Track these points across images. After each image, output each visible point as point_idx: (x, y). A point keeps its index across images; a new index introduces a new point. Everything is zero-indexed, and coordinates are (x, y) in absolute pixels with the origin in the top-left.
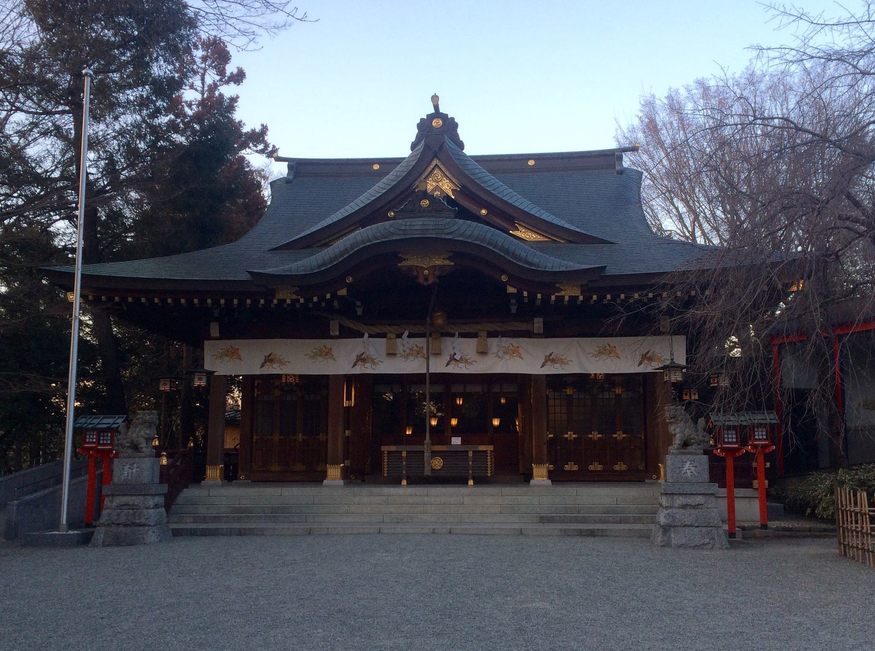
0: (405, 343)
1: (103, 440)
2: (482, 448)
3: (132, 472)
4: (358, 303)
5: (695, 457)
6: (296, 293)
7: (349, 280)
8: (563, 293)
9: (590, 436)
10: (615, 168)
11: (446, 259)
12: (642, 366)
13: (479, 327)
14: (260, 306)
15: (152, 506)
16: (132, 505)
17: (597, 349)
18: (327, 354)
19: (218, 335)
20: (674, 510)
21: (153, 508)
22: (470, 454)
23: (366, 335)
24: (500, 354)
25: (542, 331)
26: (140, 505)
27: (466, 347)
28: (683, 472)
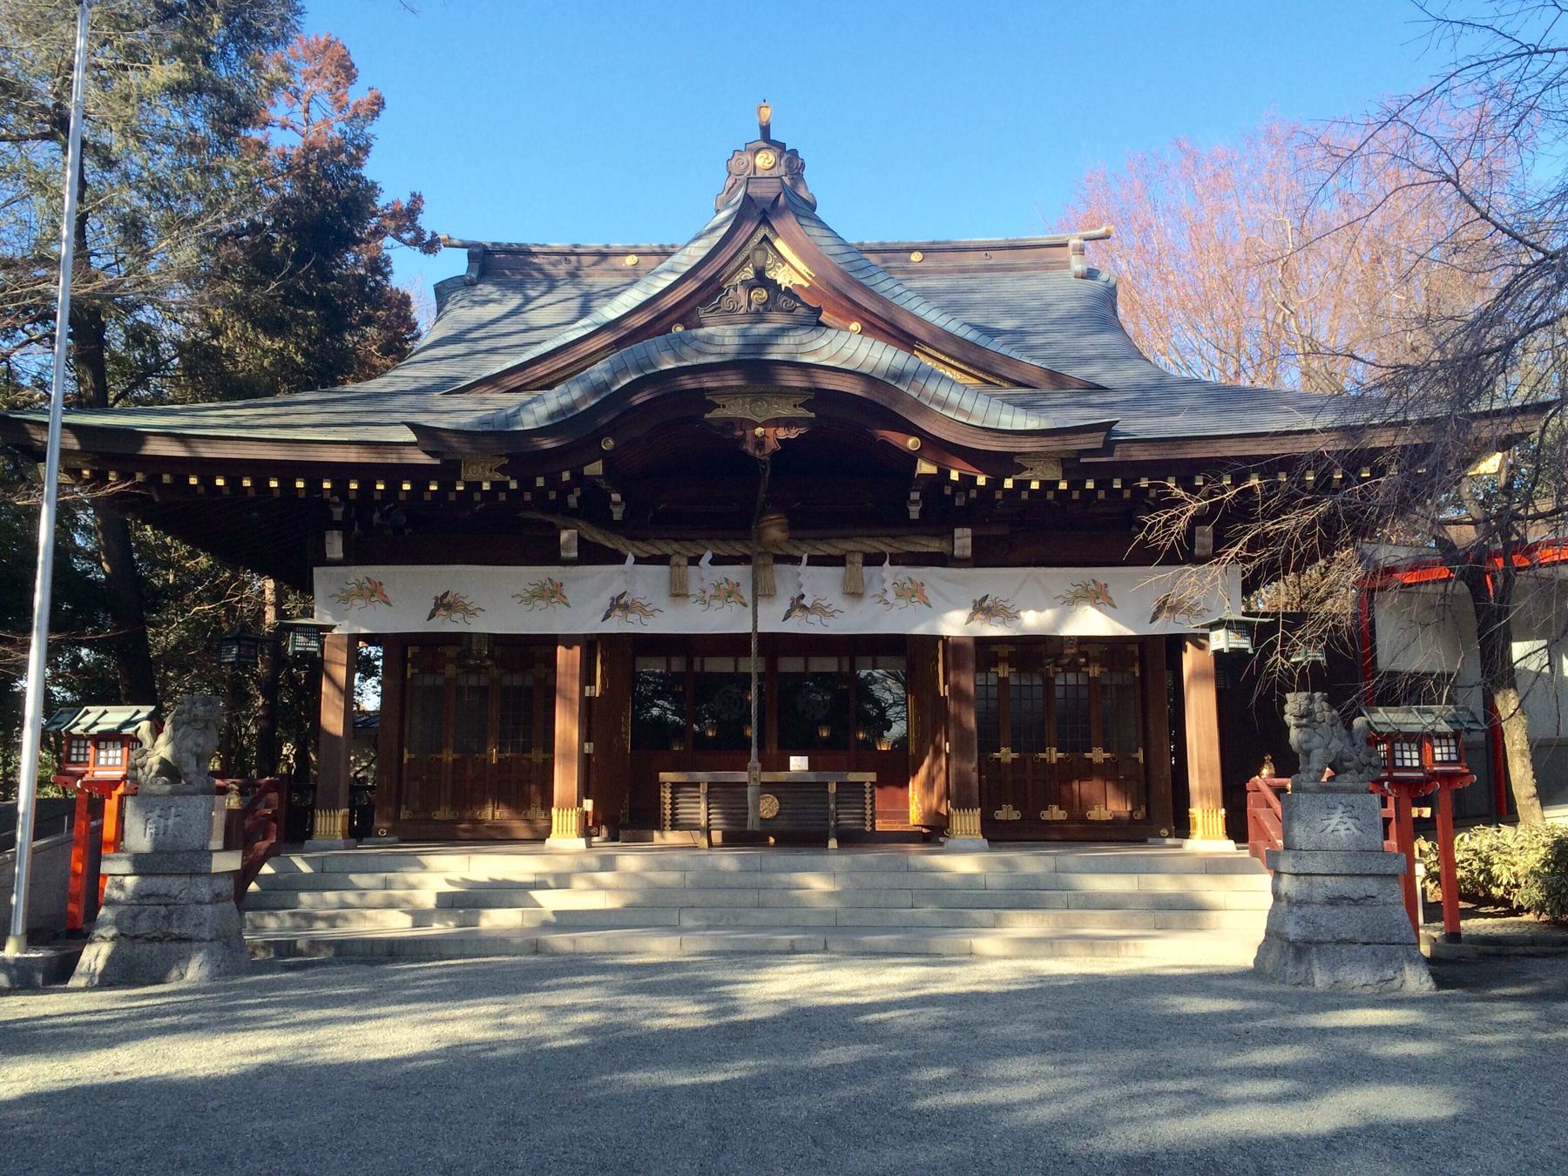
0: (706, 575)
1: (78, 755)
2: (853, 777)
3: (166, 826)
4: (616, 497)
5: (1353, 797)
6: (502, 469)
7: (608, 444)
8: (1025, 475)
9: (1042, 755)
10: (1068, 267)
11: (801, 405)
12: (1158, 622)
13: (848, 546)
14: (427, 497)
15: (207, 898)
16: (166, 895)
17: (1073, 589)
18: (553, 593)
19: (341, 555)
20: (1316, 909)
21: (211, 903)
22: (832, 788)
23: (631, 558)
24: (890, 596)
25: (968, 553)
26: (182, 895)
27: (821, 583)
28: (1330, 829)
